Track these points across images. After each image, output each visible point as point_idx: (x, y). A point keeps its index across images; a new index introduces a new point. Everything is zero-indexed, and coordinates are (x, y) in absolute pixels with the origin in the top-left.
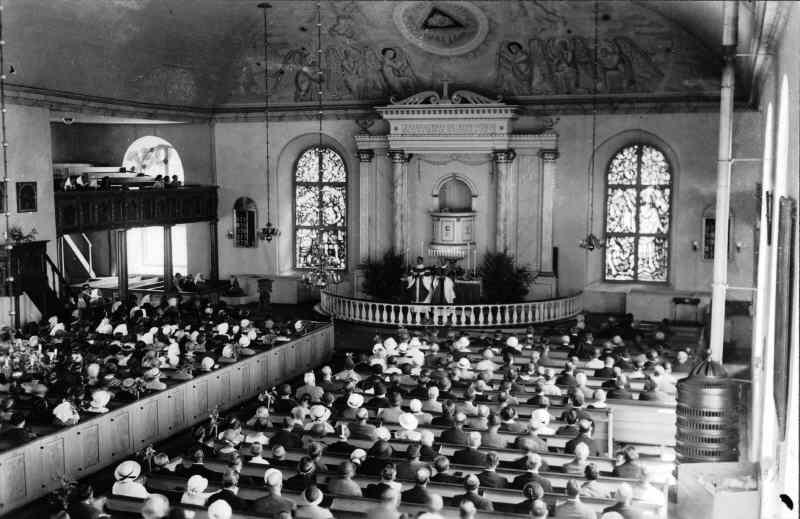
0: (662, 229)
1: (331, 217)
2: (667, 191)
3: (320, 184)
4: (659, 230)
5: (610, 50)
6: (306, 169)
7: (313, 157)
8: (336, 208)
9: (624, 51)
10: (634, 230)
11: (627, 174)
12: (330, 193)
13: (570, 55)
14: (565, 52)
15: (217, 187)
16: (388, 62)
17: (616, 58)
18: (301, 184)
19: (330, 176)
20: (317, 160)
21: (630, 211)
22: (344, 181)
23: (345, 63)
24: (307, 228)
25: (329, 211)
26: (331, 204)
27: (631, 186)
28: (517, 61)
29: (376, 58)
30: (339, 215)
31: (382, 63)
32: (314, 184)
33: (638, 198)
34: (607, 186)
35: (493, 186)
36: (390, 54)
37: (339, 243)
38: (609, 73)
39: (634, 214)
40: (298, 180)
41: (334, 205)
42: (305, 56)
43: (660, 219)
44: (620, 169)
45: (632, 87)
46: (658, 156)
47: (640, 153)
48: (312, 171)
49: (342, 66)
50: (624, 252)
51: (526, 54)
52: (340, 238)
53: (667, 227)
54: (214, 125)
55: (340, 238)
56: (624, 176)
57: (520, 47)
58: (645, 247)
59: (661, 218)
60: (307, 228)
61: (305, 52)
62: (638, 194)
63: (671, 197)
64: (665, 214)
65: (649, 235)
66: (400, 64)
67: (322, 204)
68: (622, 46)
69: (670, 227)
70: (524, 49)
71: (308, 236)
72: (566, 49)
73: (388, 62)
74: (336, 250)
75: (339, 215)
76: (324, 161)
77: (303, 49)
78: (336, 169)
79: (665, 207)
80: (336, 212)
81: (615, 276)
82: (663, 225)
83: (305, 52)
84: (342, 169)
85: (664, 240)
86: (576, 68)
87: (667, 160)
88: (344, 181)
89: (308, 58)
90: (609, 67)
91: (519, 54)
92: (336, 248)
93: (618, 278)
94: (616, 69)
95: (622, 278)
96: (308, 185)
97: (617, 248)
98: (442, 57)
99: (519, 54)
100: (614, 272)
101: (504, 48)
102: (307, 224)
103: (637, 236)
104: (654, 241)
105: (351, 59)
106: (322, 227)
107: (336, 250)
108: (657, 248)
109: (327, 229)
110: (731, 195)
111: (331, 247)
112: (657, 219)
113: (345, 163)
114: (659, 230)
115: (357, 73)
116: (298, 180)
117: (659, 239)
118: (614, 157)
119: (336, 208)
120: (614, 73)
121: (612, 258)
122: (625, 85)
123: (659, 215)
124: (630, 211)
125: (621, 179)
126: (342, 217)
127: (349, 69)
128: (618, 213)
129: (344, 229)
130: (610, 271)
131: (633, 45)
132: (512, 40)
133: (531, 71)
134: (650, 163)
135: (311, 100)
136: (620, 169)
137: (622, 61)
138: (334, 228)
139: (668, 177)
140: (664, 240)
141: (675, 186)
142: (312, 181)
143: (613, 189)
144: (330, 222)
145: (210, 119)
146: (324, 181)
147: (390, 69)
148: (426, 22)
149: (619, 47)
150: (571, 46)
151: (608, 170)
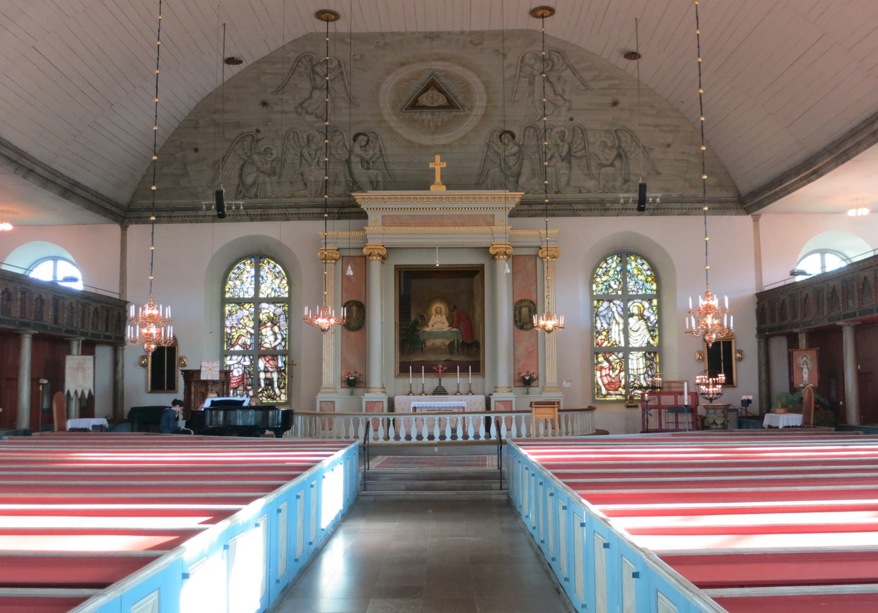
0: (652, 342)
1: (269, 339)
2: (655, 302)
3: (256, 301)
4: (648, 343)
5: (609, 144)
6: (238, 282)
7: (248, 268)
8: (276, 329)
9: (623, 145)
10: (623, 344)
11: (612, 283)
12: (267, 310)
13: (566, 148)
14: (561, 144)
15: (126, 302)
16: (357, 150)
17: (614, 153)
18: (231, 301)
19: (269, 291)
20: (253, 272)
21: (617, 323)
22: (286, 295)
23: (305, 151)
24: (238, 353)
25: (266, 331)
26: (269, 324)
27: (617, 297)
28: (507, 154)
29: (345, 145)
30: (279, 337)
31: (351, 152)
32: (248, 301)
33: (626, 309)
34: (593, 297)
35: (119, 376)
36: (362, 140)
37: (279, 371)
38: (603, 170)
39: (622, 326)
40: (227, 296)
41: (275, 325)
42: (258, 140)
43: (650, 331)
44: (605, 278)
45: (626, 186)
46: (643, 264)
47: (623, 263)
48: (247, 284)
49: (302, 155)
50: (613, 369)
51: (518, 145)
52: (280, 364)
53: (657, 339)
54: (127, 227)
55: (280, 364)
56: (610, 286)
57: (513, 136)
58: (635, 361)
59: (651, 330)
60: (238, 353)
61: (260, 136)
62: (625, 305)
63: (659, 307)
64: (654, 326)
65: (440, 383)
66: (371, 152)
67: (259, 324)
68: (623, 139)
69: (660, 336)
70: (517, 140)
71: (239, 363)
72: (563, 140)
73: (357, 150)
74: (275, 380)
75: (279, 337)
76: (262, 273)
77: (258, 131)
78: (277, 281)
79: (653, 318)
80: (275, 334)
81: (605, 396)
82: (653, 337)
83: (260, 136)
84: (284, 282)
85: (655, 353)
86: (570, 163)
87: (653, 268)
88: (286, 295)
89: (260, 144)
90: (605, 162)
91: (511, 145)
92: (275, 376)
93: (608, 398)
94: (612, 165)
95: (614, 398)
96: (240, 302)
97: (606, 364)
98: (421, 146)
99: (511, 145)
100: (604, 391)
101: (496, 134)
102: (238, 348)
103: (627, 350)
104: (645, 354)
105: (313, 147)
106: (257, 351)
107: (275, 380)
108: (648, 363)
109: (263, 355)
110: (400, 362)
111: (269, 375)
112: (646, 332)
113: (288, 275)
114: (648, 343)
115: (318, 163)
116: (227, 296)
117: (650, 354)
118: (598, 266)
119: (276, 329)
120: (609, 170)
121: (601, 377)
122: (618, 183)
123: (648, 327)
124: (617, 323)
125: (607, 289)
126: (283, 339)
127: (309, 158)
128: (605, 326)
129: (284, 353)
130: (600, 390)
131: (634, 138)
132: (507, 128)
133: (521, 166)
134: (636, 272)
135: (256, 196)
136: (605, 278)
137: (619, 156)
138: (273, 354)
139: (654, 287)
140: (655, 353)
141: (665, 298)
142: (246, 296)
143: (598, 301)
144: (268, 346)
145: (124, 218)
146: (261, 296)
147: (358, 159)
148: (416, 101)
149: (620, 142)
150: (568, 138)
151: (592, 281)
